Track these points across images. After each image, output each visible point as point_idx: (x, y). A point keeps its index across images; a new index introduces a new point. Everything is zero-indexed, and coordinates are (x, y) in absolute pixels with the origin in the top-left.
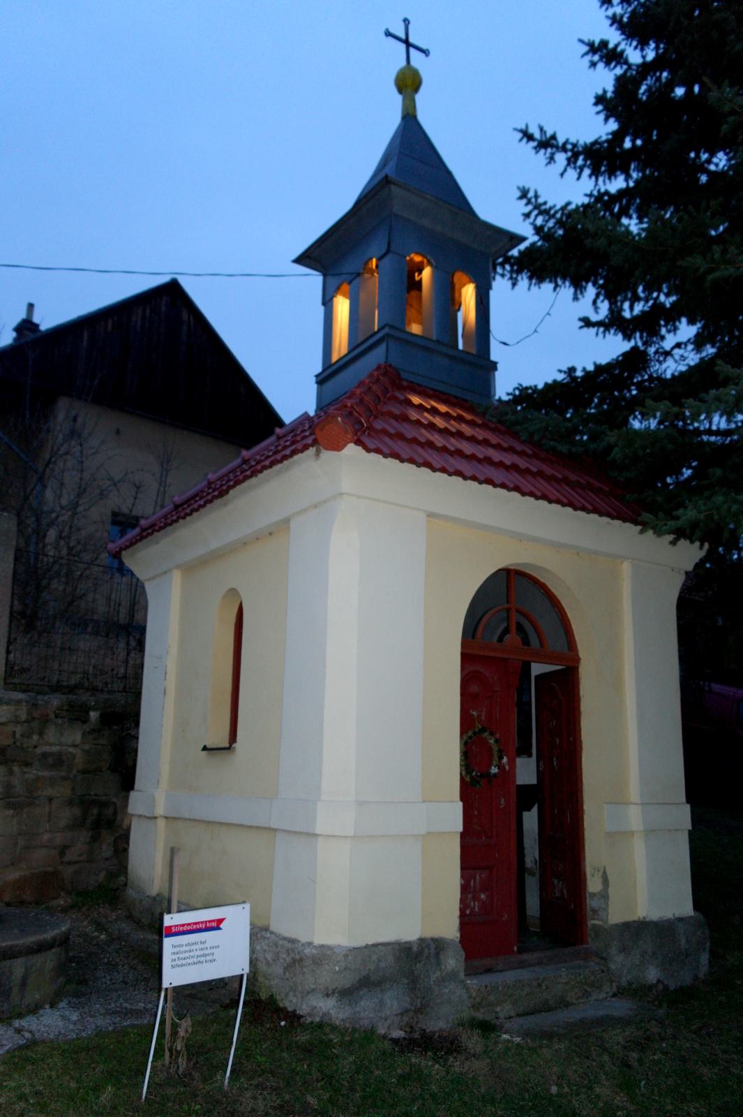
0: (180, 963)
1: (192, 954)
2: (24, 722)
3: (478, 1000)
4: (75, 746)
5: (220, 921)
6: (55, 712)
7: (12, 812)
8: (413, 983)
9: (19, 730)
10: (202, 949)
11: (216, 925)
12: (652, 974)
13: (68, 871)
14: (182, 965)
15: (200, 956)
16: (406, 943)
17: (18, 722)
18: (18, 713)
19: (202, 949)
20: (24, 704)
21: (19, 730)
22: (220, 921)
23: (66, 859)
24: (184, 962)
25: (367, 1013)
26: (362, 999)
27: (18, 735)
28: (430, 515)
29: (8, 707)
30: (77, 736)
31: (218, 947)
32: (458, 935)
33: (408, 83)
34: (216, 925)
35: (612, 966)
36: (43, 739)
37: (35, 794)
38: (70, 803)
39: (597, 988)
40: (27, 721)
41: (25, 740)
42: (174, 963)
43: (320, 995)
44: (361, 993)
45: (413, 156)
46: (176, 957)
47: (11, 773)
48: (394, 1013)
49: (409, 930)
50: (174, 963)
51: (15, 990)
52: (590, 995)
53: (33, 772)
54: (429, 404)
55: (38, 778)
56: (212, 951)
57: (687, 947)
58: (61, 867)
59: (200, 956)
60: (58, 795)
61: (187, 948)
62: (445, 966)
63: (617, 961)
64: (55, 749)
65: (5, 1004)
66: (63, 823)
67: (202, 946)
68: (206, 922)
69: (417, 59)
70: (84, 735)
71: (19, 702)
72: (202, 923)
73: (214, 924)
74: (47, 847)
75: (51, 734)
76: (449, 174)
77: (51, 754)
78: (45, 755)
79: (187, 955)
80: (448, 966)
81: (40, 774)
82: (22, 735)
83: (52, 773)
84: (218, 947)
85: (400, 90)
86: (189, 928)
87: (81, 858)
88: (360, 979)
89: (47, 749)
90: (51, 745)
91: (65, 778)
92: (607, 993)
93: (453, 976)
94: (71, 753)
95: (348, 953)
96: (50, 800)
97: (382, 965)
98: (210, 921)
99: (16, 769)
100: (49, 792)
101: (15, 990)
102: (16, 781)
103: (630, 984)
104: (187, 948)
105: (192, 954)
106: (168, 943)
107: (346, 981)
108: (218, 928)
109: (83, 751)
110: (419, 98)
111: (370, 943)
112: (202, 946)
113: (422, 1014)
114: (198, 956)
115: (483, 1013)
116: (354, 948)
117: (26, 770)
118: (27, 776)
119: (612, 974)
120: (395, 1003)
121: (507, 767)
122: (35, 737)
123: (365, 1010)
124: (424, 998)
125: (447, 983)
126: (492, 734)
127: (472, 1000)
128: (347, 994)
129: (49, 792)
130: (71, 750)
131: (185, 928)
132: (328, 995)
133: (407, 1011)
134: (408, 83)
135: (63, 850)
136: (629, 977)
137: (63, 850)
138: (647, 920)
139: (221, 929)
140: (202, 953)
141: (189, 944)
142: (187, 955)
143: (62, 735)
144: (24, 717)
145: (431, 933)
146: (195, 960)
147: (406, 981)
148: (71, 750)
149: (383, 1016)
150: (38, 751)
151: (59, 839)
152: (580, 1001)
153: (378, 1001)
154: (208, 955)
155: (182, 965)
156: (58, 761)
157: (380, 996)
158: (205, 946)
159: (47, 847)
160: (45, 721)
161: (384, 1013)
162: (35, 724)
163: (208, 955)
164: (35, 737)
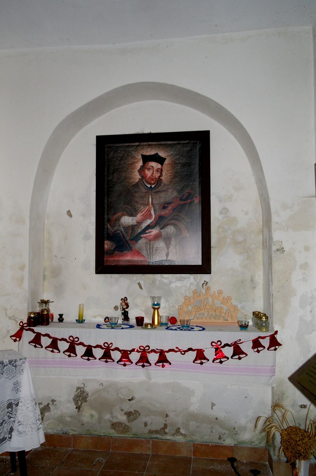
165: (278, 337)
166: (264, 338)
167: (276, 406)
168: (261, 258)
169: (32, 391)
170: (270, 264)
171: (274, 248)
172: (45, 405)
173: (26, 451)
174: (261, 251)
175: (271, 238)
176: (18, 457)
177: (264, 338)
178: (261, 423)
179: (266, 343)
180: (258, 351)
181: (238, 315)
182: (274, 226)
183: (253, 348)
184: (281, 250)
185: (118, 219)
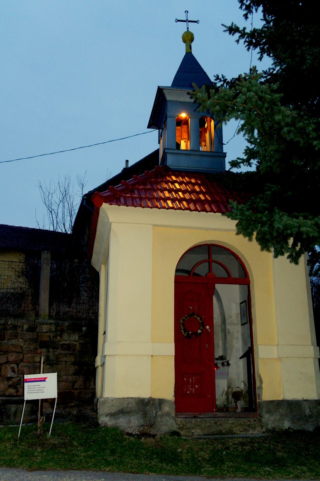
0: (31, 392)
1: (35, 389)
2: (54, 332)
3: (181, 426)
4: (75, 341)
5: (46, 378)
6: (67, 328)
7: (49, 366)
8: (145, 415)
9: (52, 335)
10: (39, 388)
11: (44, 380)
12: (286, 425)
13: (76, 392)
14: (31, 393)
15: (38, 390)
16: (143, 398)
17: (51, 332)
18: (51, 328)
19: (39, 388)
20: (53, 324)
21: (52, 335)
22: (46, 378)
23: (75, 387)
24: (32, 392)
25: (122, 424)
26: (120, 418)
27: (51, 337)
28: (154, 225)
29: (47, 326)
30: (76, 337)
31: (45, 387)
32: (174, 399)
33: (188, 38)
34: (44, 380)
35: (263, 420)
36: (62, 338)
37: (58, 360)
38: (74, 364)
39: (252, 428)
40: (55, 331)
41: (55, 339)
42: (28, 392)
43: (104, 416)
44: (120, 415)
45: (190, 71)
46: (29, 390)
47: (49, 351)
48: (136, 425)
49: (145, 392)
50: (28, 392)
51: (12, 416)
52: (248, 431)
53: (58, 352)
54: (183, 179)
55: (60, 354)
56: (42, 389)
57: (310, 414)
58: (73, 391)
59: (38, 390)
60: (69, 361)
61: (33, 387)
62: (164, 410)
63: (266, 417)
64: (67, 342)
65: (8, 420)
66: (71, 372)
67: (38, 387)
68: (40, 378)
69: (193, 27)
70: (79, 337)
71: (51, 324)
72: (38, 378)
73: (43, 379)
74: (65, 381)
75: (65, 336)
76: (205, 73)
77: (65, 344)
78: (63, 345)
79: (33, 389)
80: (165, 410)
81: (61, 352)
82: (53, 337)
83: (66, 352)
84: (45, 387)
85: (184, 41)
86: (33, 380)
87: (81, 387)
88: (119, 410)
89: (64, 342)
90: (66, 341)
91: (71, 354)
92: (259, 431)
93: (168, 414)
94: (74, 344)
95: (114, 399)
96: (66, 362)
97: (130, 406)
98: (41, 378)
99: (51, 350)
100: (65, 359)
101: (12, 416)
102: (51, 355)
103: (274, 429)
104: (33, 387)
105: (35, 389)
106: (26, 385)
107: (113, 410)
108: (44, 381)
109: (80, 343)
110: (193, 44)
111: (125, 397)
112: (38, 387)
113: (152, 428)
114: (37, 390)
115: (185, 432)
116: (117, 398)
117: (55, 350)
118: (56, 353)
119: (263, 423)
120: (136, 422)
121: (209, 331)
122: (59, 338)
123: (121, 423)
124: (150, 421)
125: (165, 417)
126: (198, 316)
127: (178, 425)
128: (112, 415)
129: (65, 359)
130: (74, 343)
131: (32, 380)
132: (106, 416)
133: (142, 426)
134: (188, 38)
135: (74, 383)
136: (273, 425)
137: (74, 383)
138: (285, 399)
139: (45, 381)
140: (39, 389)
141: (33, 386)
142: (33, 389)
143: (70, 337)
144: (54, 330)
145: (157, 396)
146: (36, 391)
147: (142, 413)
148: (74, 343)
149: (130, 426)
150: (60, 343)
151: (70, 378)
152: (242, 433)
153: (128, 420)
154: (41, 390)
155: (31, 393)
156: (68, 347)
157: (129, 418)
158: (40, 387)
159: (65, 381)
160: (62, 332)
161: (132, 424)
162: (58, 332)
163: (41, 390)
164: (59, 338)
165: (229, 362)
166: (225, 362)
167: (229, 387)
168: (220, 336)
169: (182, 99)
170: (225, 338)
171: (227, 331)
172: (91, 472)
173: (125, 167)
174: (220, 333)
175: (225, 328)
176: (198, 320)
177: (225, 362)
178: (225, 392)
179: (226, 364)
180: (224, 366)
181: (75, 413)
182: (227, 324)
183: (222, 365)
184: (229, 332)
185: (268, 104)
